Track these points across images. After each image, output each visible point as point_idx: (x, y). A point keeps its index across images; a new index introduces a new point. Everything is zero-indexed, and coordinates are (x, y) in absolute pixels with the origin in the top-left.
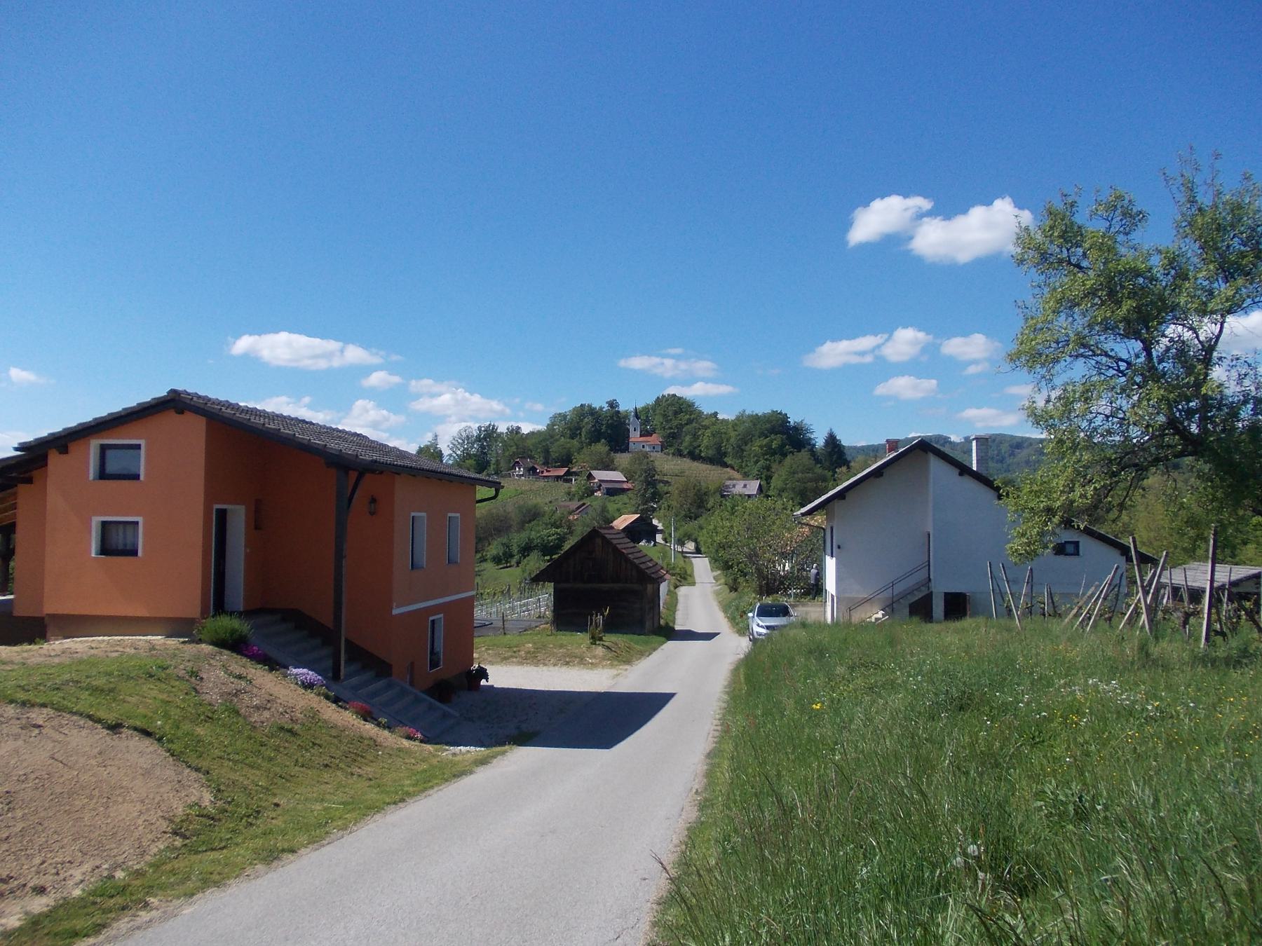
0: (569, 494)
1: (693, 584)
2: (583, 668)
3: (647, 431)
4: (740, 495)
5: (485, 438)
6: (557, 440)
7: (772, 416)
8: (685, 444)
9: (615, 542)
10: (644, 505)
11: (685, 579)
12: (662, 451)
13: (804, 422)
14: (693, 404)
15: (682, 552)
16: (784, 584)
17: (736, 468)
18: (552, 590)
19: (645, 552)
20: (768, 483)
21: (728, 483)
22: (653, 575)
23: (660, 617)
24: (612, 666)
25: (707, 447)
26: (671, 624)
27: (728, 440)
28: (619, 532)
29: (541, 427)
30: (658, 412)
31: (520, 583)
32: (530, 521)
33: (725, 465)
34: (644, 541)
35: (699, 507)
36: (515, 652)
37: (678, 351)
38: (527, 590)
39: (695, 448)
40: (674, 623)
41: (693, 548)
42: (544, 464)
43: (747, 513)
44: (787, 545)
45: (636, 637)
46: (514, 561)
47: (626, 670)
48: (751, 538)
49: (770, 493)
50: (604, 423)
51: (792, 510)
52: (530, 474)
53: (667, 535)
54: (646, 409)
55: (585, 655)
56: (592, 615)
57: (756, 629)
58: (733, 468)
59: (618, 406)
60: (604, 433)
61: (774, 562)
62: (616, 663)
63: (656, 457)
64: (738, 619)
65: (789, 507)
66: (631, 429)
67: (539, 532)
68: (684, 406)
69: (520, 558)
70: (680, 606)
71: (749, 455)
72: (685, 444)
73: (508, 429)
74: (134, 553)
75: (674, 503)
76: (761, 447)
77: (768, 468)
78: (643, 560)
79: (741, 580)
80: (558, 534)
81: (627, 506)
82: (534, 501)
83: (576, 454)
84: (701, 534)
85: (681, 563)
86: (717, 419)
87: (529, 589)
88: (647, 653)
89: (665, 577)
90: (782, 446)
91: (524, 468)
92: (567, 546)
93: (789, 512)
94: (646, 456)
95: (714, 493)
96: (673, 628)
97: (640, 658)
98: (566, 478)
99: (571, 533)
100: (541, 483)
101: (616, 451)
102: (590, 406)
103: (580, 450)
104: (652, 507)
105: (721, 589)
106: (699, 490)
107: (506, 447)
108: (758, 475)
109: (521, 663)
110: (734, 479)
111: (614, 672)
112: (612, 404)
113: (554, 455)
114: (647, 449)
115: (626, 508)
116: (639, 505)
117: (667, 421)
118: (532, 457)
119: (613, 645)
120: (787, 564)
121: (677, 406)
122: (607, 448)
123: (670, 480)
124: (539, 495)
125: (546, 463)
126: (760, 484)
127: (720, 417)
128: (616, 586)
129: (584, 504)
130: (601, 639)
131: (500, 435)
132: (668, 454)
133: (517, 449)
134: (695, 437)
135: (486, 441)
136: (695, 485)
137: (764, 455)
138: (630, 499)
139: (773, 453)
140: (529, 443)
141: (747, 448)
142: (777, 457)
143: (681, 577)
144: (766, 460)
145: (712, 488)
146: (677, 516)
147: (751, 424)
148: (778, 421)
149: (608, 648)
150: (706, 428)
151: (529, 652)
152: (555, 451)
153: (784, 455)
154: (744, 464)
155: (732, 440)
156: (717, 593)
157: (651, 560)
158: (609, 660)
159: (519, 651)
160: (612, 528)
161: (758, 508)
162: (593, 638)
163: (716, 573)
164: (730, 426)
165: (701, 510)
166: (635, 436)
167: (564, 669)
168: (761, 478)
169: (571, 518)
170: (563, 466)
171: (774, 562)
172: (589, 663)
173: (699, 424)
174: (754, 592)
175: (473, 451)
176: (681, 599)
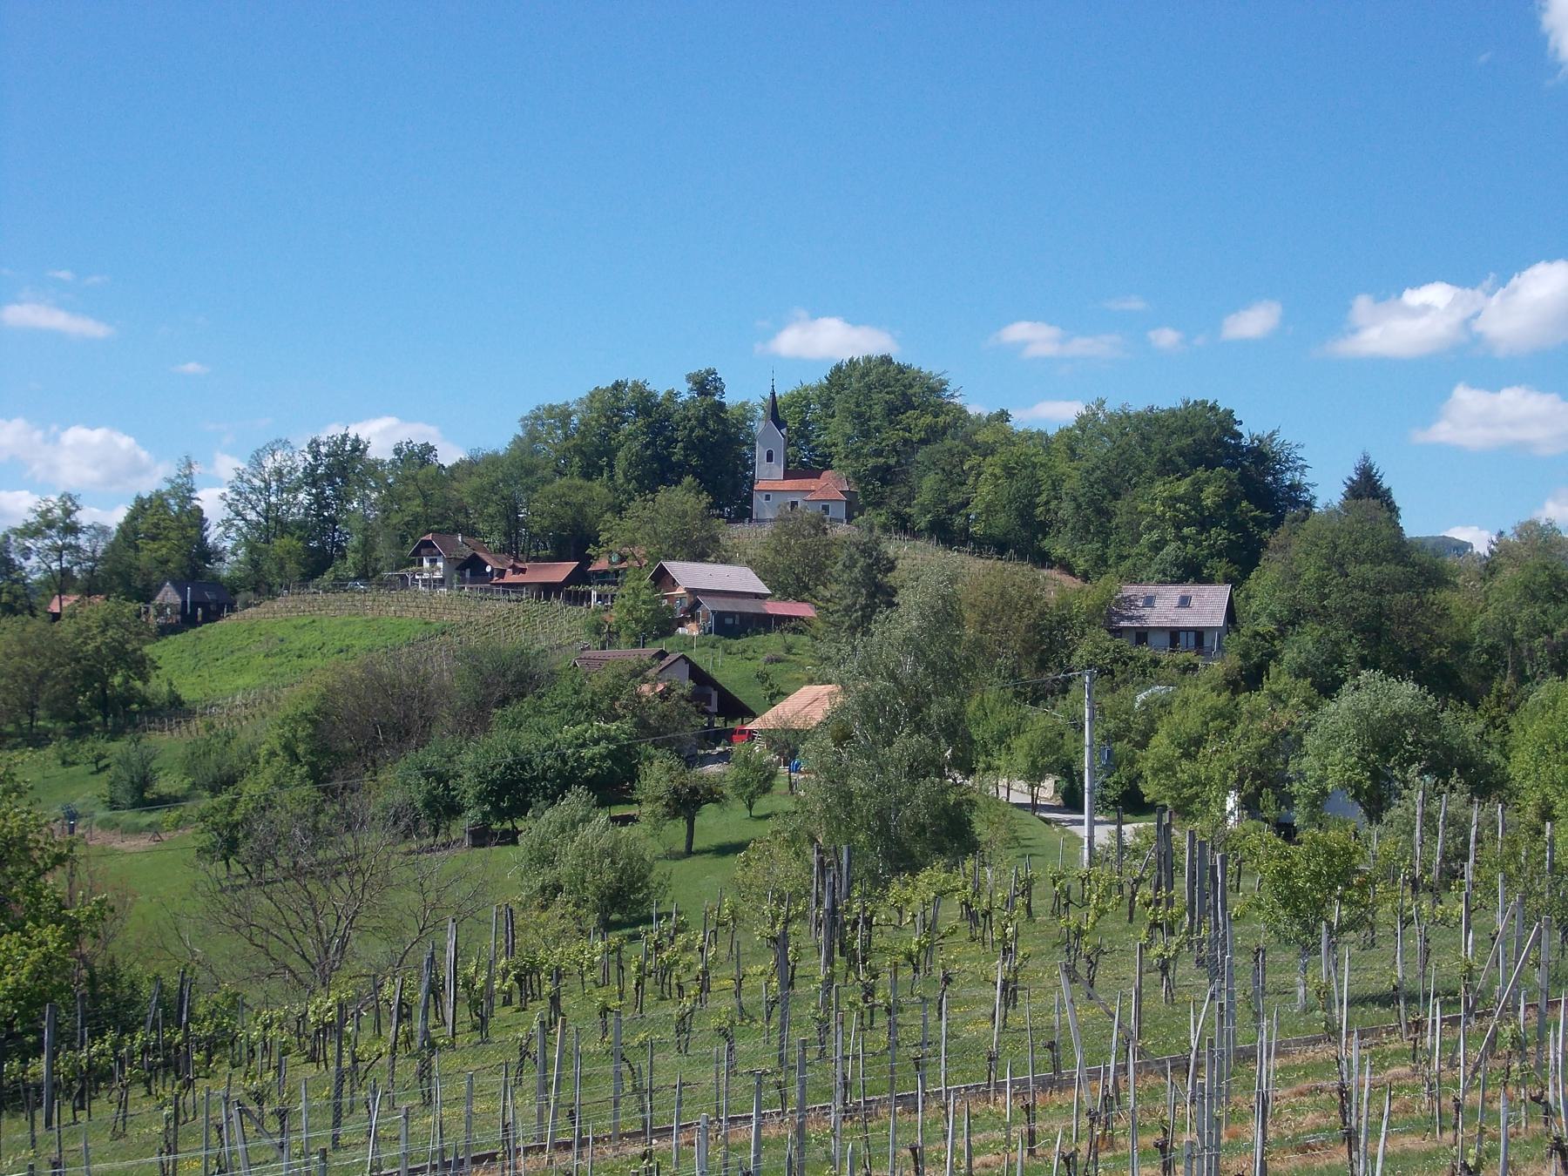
5: (329, 476)
6: (546, 481)
12: (850, 518)
13: (1279, 438)
25: (989, 509)
30: (836, 408)
32: (504, 702)
33: (1043, 559)
39: (951, 511)
42: (502, 550)
46: (461, 827)
50: (679, 435)
52: (462, 580)
54: (801, 400)
58: (1068, 569)
59: (720, 389)
66: (760, 453)
67: (545, 732)
68: (916, 389)
73: (398, 451)
91: (447, 561)
98: (572, 592)
107: (393, 498)
112: (705, 384)
118: (471, 532)
121: (898, 389)
131: (373, 468)
134: (954, 478)
135: (332, 483)
140: (463, 490)
141: (1121, 506)
150: (988, 451)
152: (536, 511)
166: (768, 476)
170: (560, 557)
175: (296, 514)
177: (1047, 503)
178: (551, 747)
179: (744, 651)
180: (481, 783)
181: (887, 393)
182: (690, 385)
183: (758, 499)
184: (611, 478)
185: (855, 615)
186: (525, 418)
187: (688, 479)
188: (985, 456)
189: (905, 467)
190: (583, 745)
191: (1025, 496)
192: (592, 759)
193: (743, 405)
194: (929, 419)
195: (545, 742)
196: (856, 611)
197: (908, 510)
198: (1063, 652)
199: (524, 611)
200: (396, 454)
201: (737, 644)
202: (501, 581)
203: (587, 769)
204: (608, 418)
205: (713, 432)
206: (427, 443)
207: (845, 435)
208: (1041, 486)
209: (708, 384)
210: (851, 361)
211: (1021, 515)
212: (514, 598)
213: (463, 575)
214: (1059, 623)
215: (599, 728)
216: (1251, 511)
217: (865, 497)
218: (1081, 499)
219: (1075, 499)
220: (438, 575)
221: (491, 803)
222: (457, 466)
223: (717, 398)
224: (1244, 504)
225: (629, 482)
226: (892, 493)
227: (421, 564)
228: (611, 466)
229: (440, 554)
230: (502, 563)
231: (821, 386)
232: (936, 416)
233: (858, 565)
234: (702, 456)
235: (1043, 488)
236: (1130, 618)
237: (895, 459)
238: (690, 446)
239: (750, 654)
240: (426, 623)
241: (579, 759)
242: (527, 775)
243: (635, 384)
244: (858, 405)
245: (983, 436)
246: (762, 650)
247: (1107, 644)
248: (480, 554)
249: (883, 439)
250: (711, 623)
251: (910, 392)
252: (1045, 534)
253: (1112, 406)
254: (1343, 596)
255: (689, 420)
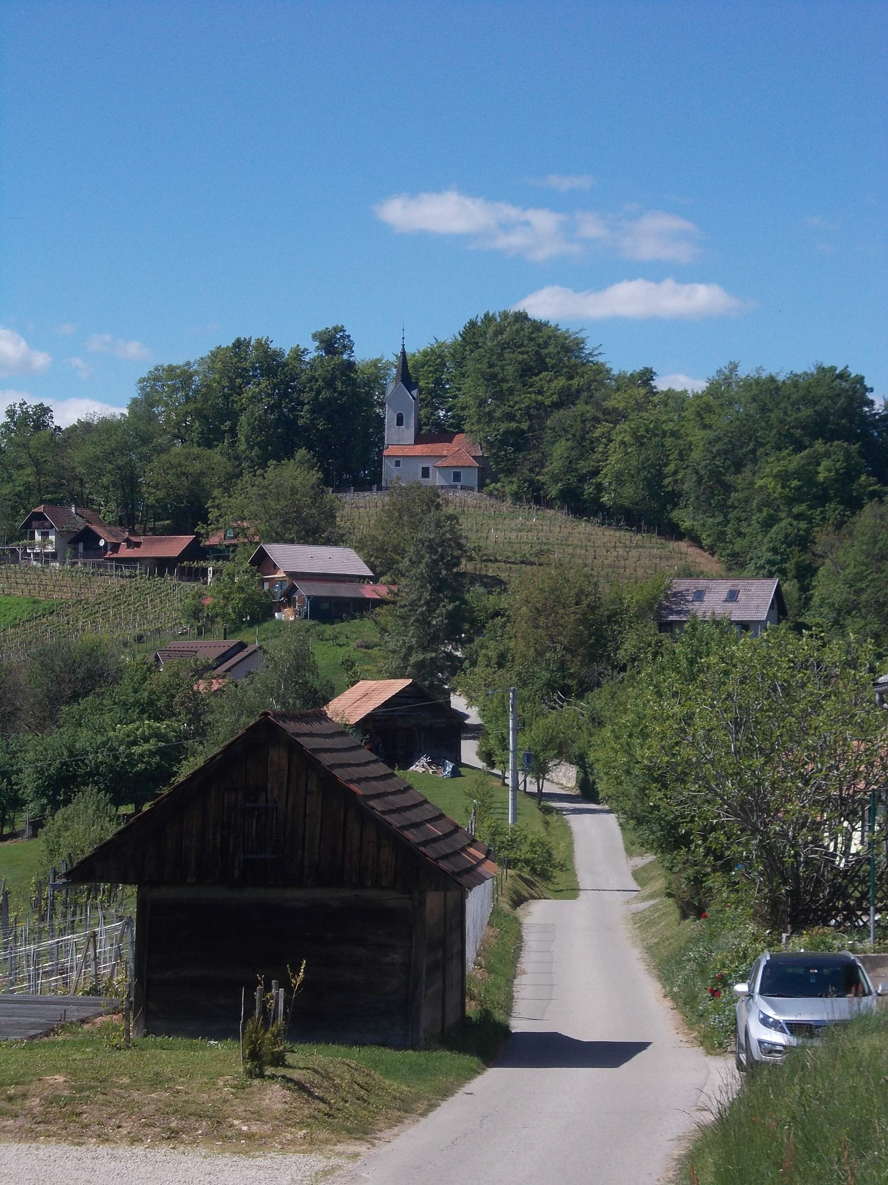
0: (196, 613)
1: (572, 892)
2: (223, 1151)
3: (438, 424)
4: (717, 623)
6: (161, 450)
7: (818, 383)
8: (555, 465)
9: (326, 759)
10: (424, 649)
11: (545, 876)
12: (481, 486)
14: (579, 344)
15: (540, 796)
16: (845, 896)
17: (706, 542)
18: (132, 909)
19: (423, 790)
20: (804, 589)
21: (682, 585)
22: (443, 864)
23: (463, 993)
24: (312, 1144)
25: (619, 479)
26: (499, 1016)
27: (682, 457)
28: (341, 732)
29: (119, 411)
30: (470, 365)
31: (40, 885)
32: (75, 697)
33: (674, 532)
34: (423, 760)
35: (592, 658)
36: (10, 1099)
37: (583, 182)
38: (60, 909)
39: (582, 479)
40: (508, 1011)
41: (572, 783)
42: (120, 522)
43: (735, 675)
44: (856, 775)
45: (388, 1055)
46: (22, 821)
47: (356, 1156)
48: (748, 752)
49: (807, 619)
50: (306, 397)
51: (872, 670)
52: (75, 555)
53: (493, 742)
55: (227, 1109)
56: (252, 986)
57: (759, 1033)
58: (696, 541)
59: (346, 347)
60: (306, 428)
61: (816, 826)
62: (323, 1134)
63: (464, 504)
64: (705, 1003)
65: (866, 659)
66: (389, 416)
67: (101, 730)
68: (551, 349)
69: (43, 808)
70: (529, 960)
71: (747, 501)
72: (555, 465)
74: (225, 639)
75: (517, 646)
76: (784, 477)
77: (804, 542)
78: (413, 816)
79: (715, 881)
80: (159, 736)
81: (374, 652)
82: (89, 637)
83: (216, 492)
84: (596, 740)
85: (534, 827)
86: (652, 392)
87: (66, 905)
88: (422, 1106)
89: (482, 869)
90: (848, 475)
91: (59, 534)
92: (185, 770)
93: (863, 674)
94: (432, 501)
95: (639, 616)
96: (505, 1030)
97: (400, 1120)
99: (201, 733)
100: (113, 581)
101: (341, 487)
102: (262, 346)
103: (231, 480)
104: (450, 656)
105: (654, 908)
106: (592, 608)
108: (772, 563)
109: (31, 1135)
110: (700, 575)
111: (316, 1161)
113: (150, 496)
114: (437, 479)
115: (373, 659)
116: (410, 648)
117: (499, 396)
118: (83, 502)
119: (317, 1079)
120: (857, 836)
121: (531, 348)
122: (315, 476)
123: (503, 576)
124: (105, 616)
125: (127, 521)
126: (779, 587)
127: (661, 384)
128: (332, 896)
129: (242, 646)
130: (278, 1060)
132: (501, 497)
133: (38, 473)
136: (582, 591)
137: (791, 501)
138: (384, 630)
139: (821, 498)
141: (738, 480)
142: (833, 509)
143: (533, 870)
144: (798, 517)
145: (632, 599)
146: (525, 684)
147: (753, 408)
148: (833, 399)
149: (301, 1087)
150: (616, 416)
151: (53, 1100)
153: (854, 504)
154: (729, 530)
155: (696, 455)
156: (643, 922)
157: (441, 816)
158: (301, 1124)
159: (24, 1096)
160: (323, 717)
161: (768, 662)
162: (254, 1055)
163: (640, 861)
164: (689, 414)
165: (597, 668)
167: (163, 1151)
168: (783, 572)
169: (201, 686)
170: (176, 530)
171: (816, 826)
172: (240, 1135)
173: (598, 405)
174: (753, 917)
176: (531, 939)
177: (675, 473)
178: (104, 744)
179: (336, 637)
180: (39, 778)
181: (522, 353)
182: (317, 344)
183: (388, 466)
184: (232, 444)
185: (420, 610)
186: (142, 380)
187: (302, 453)
188: (616, 422)
189: (537, 433)
190: (134, 743)
191: (653, 466)
192: (142, 755)
193: (375, 364)
194: (561, 382)
195: (100, 739)
196: (421, 606)
197: (540, 477)
198: (611, 646)
199: (137, 589)
200: (10, 416)
201: (329, 630)
202: (115, 555)
203: (136, 765)
204: (231, 380)
205: (342, 394)
206: (42, 404)
207: (477, 397)
208: (669, 455)
209: (336, 343)
210: (486, 316)
211: (650, 486)
212: (127, 574)
213: (76, 549)
214: (609, 617)
215: (149, 727)
216: (871, 485)
217: (497, 463)
218: (702, 472)
219: (697, 473)
220: (50, 549)
221: (48, 797)
222: (74, 428)
223: (345, 357)
224: (863, 478)
225: (251, 448)
226: (525, 459)
227: (33, 537)
228: (233, 431)
229: (52, 527)
230: (115, 536)
231: (454, 344)
232: (571, 378)
233: (424, 561)
234: (329, 419)
235: (670, 458)
236: (678, 613)
237: (528, 424)
238: (318, 408)
239: (342, 640)
240: (34, 602)
241: (130, 756)
242: (81, 771)
243: (259, 341)
244: (491, 366)
245: (616, 402)
246: (354, 636)
247: (650, 638)
248: (93, 527)
249: (516, 403)
250: (307, 608)
251: (544, 352)
252: (676, 505)
253: (745, 371)
254: (878, 591)
255: (317, 381)
